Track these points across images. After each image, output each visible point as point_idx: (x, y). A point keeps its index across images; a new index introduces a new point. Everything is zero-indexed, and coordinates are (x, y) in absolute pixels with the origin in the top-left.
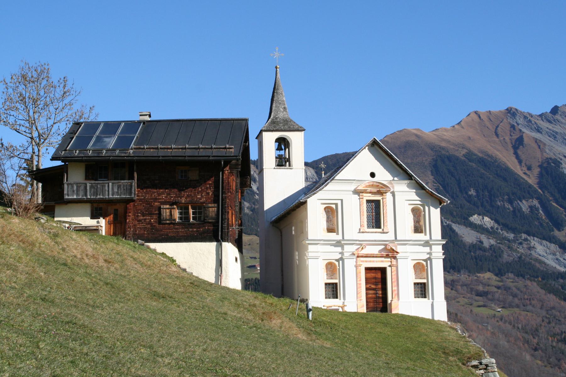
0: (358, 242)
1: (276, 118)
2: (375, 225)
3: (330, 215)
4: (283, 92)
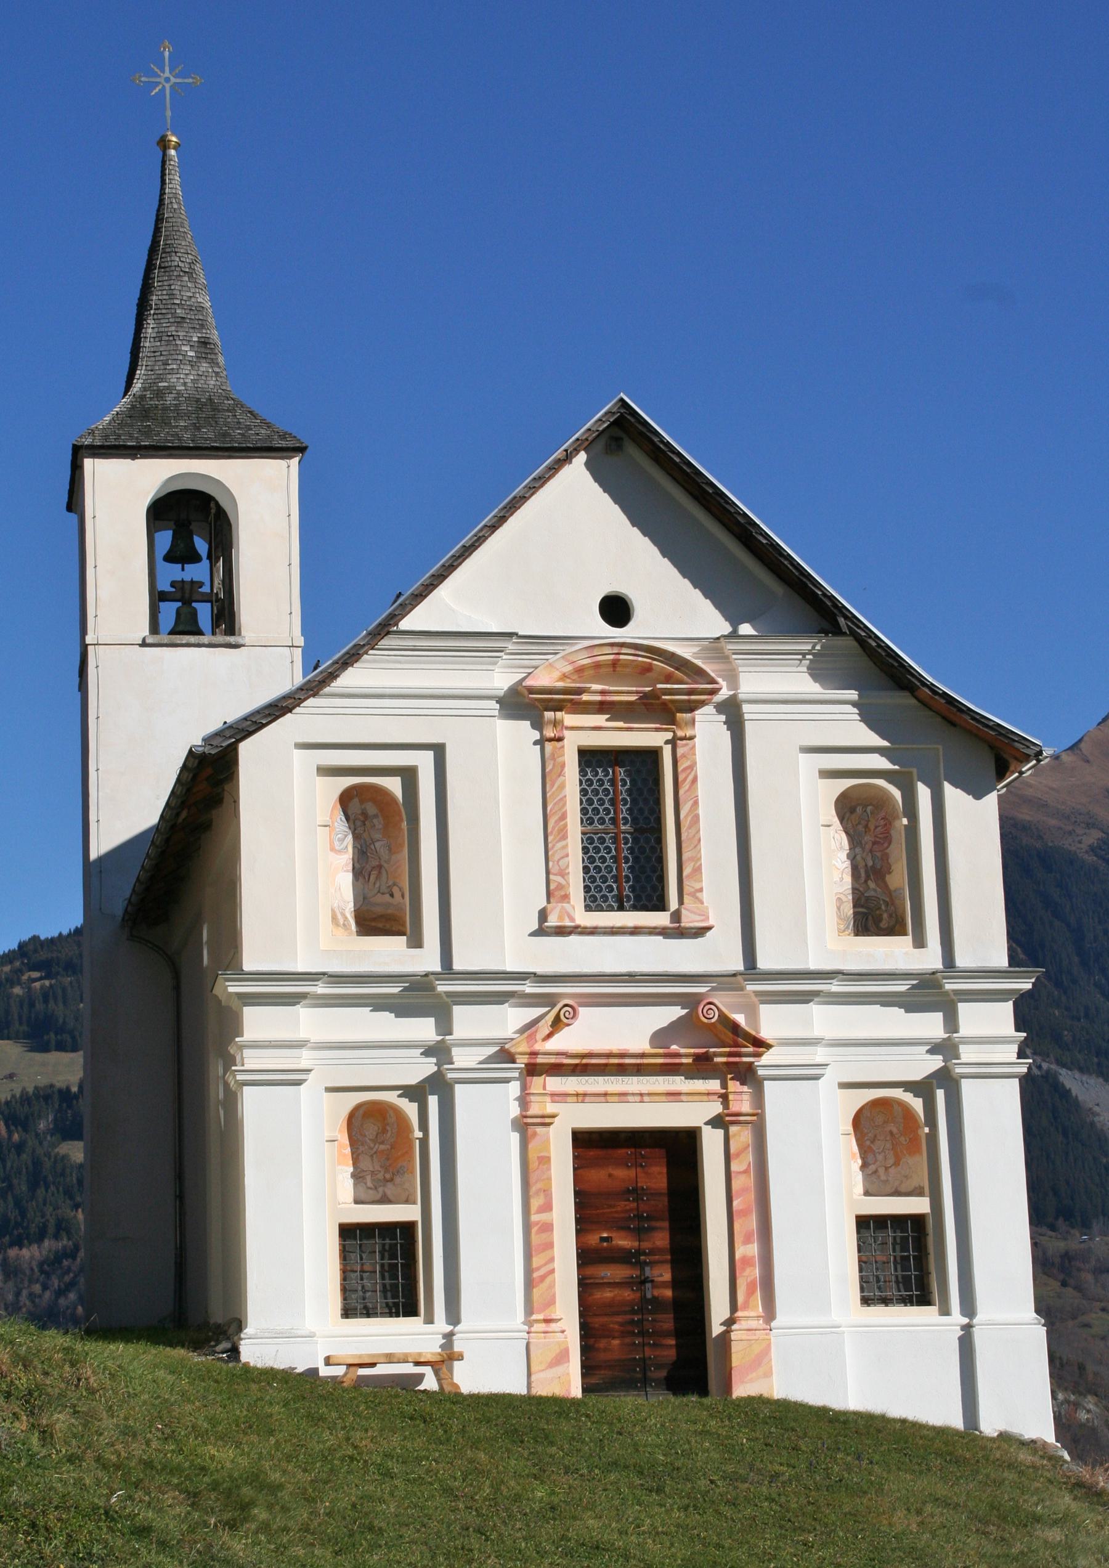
0: (529, 988)
1: (160, 394)
2: (633, 889)
3: (377, 836)
4: (198, 267)
